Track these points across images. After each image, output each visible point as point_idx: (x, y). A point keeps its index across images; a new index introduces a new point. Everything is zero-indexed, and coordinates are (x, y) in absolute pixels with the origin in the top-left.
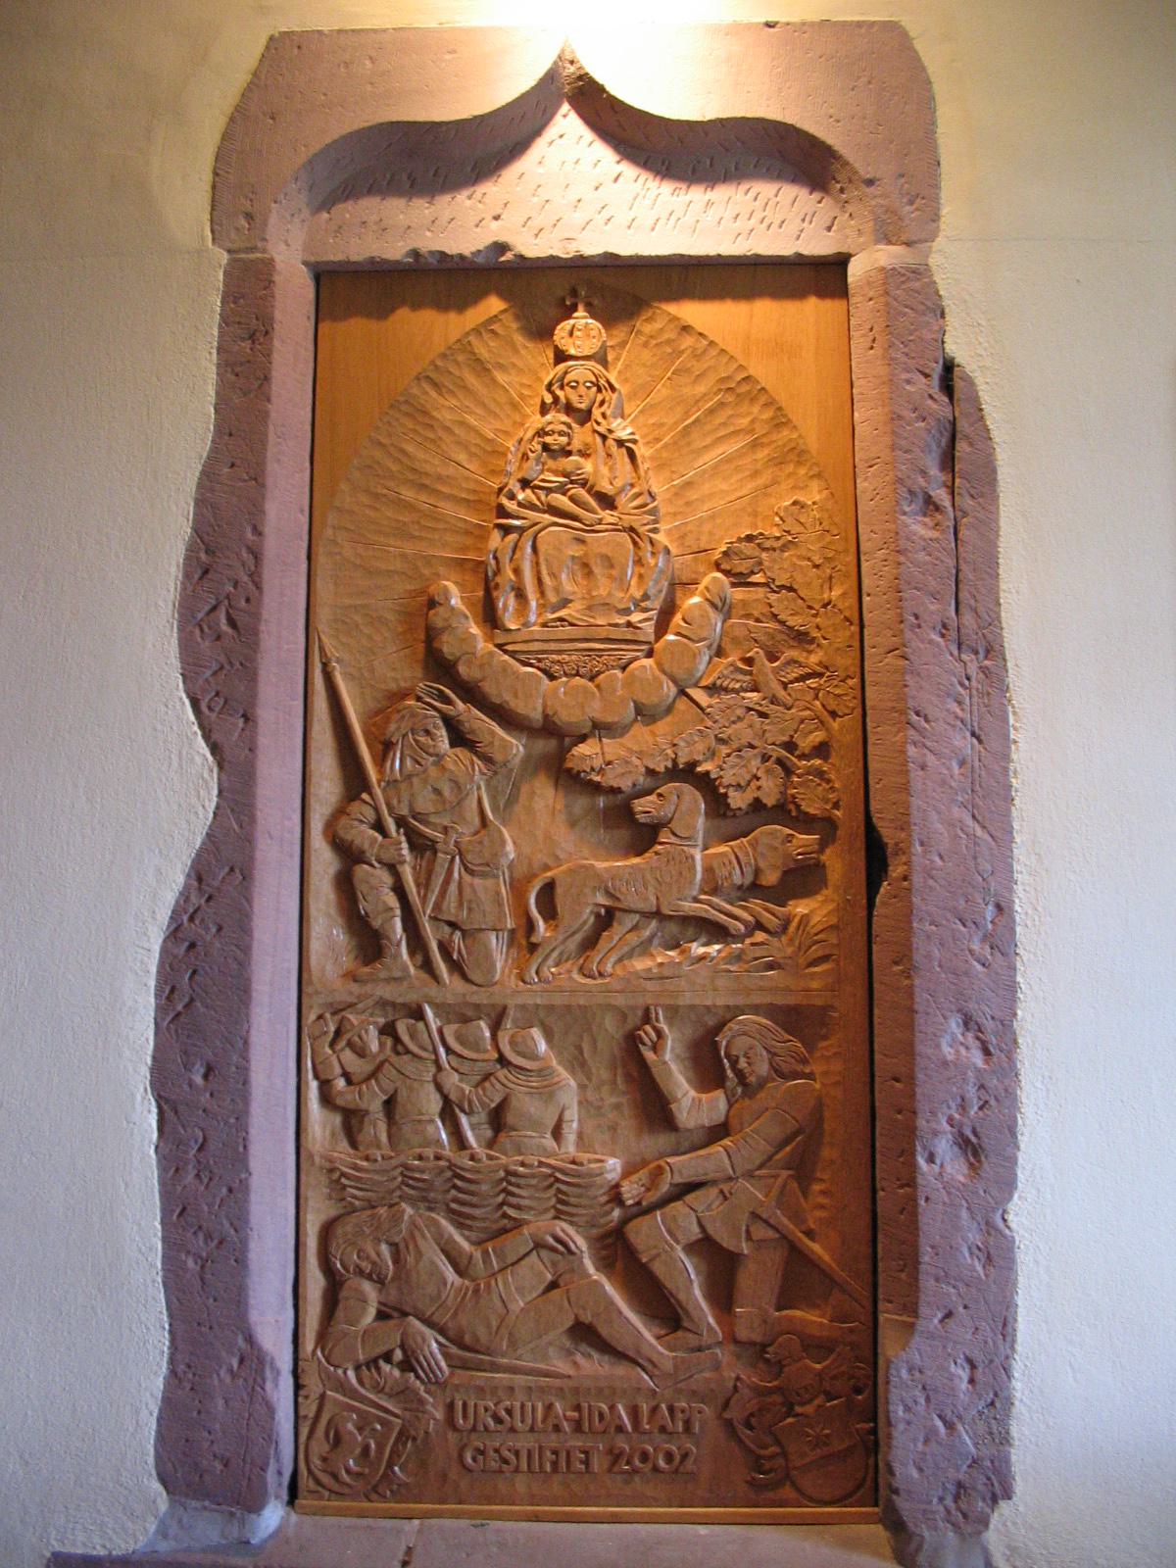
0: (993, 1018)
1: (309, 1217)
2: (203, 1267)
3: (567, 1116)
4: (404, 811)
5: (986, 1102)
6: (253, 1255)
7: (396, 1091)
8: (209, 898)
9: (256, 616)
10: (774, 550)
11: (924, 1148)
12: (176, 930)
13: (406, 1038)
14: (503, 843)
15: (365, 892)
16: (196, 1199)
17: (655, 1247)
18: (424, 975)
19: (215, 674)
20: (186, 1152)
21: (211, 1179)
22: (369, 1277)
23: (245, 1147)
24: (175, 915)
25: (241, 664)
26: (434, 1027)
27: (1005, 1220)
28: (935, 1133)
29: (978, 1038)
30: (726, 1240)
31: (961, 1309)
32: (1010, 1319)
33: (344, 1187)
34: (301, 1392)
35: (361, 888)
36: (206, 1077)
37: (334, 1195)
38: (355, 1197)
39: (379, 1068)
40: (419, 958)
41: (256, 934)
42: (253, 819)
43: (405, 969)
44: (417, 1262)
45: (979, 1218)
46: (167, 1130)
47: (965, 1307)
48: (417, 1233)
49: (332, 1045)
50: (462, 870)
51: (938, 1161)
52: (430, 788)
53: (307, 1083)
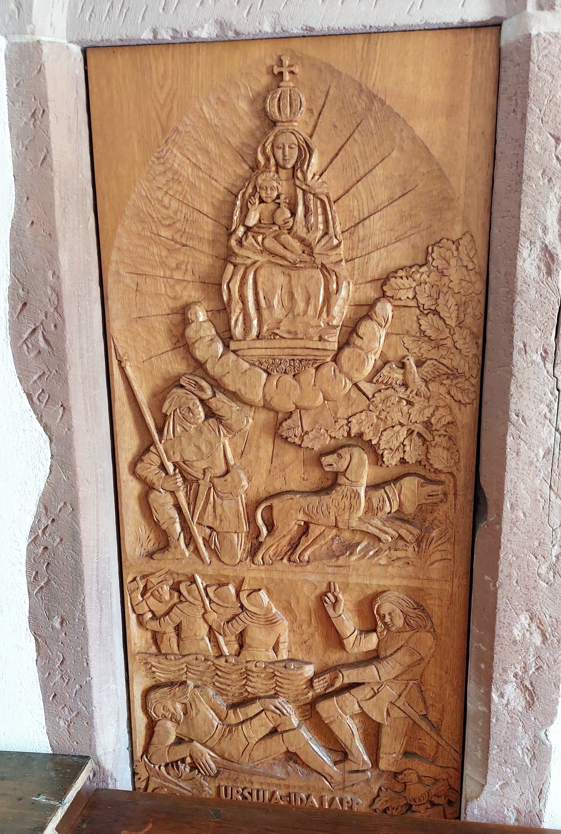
0: (550, 617)
1: (135, 687)
2: (69, 726)
3: (281, 640)
4: (178, 459)
5: (541, 667)
6: (97, 720)
7: (181, 622)
8: (53, 520)
9: (62, 338)
10: (424, 804)
11: (497, 690)
12: (35, 538)
13: (185, 593)
14: (240, 481)
15: (156, 508)
16: (62, 690)
17: (333, 716)
18: (194, 557)
19: (40, 377)
20: (54, 665)
21: (69, 680)
22: (171, 720)
23: (87, 664)
24: (33, 530)
25: (57, 371)
26: (201, 587)
27: (546, 736)
28: (505, 682)
29: (539, 628)
30: (375, 716)
31: (514, 781)
32: (544, 790)
33: (154, 672)
34: (137, 777)
35: (154, 505)
36: (62, 623)
37: (148, 675)
38: (159, 677)
39: (171, 609)
40: (192, 547)
41: (84, 543)
42: (75, 474)
43: (183, 554)
44: (197, 714)
45: (530, 733)
46: (42, 652)
47: (517, 781)
48: (196, 698)
49: (143, 595)
50: (216, 496)
51: (506, 698)
52: (193, 445)
53: (129, 616)
